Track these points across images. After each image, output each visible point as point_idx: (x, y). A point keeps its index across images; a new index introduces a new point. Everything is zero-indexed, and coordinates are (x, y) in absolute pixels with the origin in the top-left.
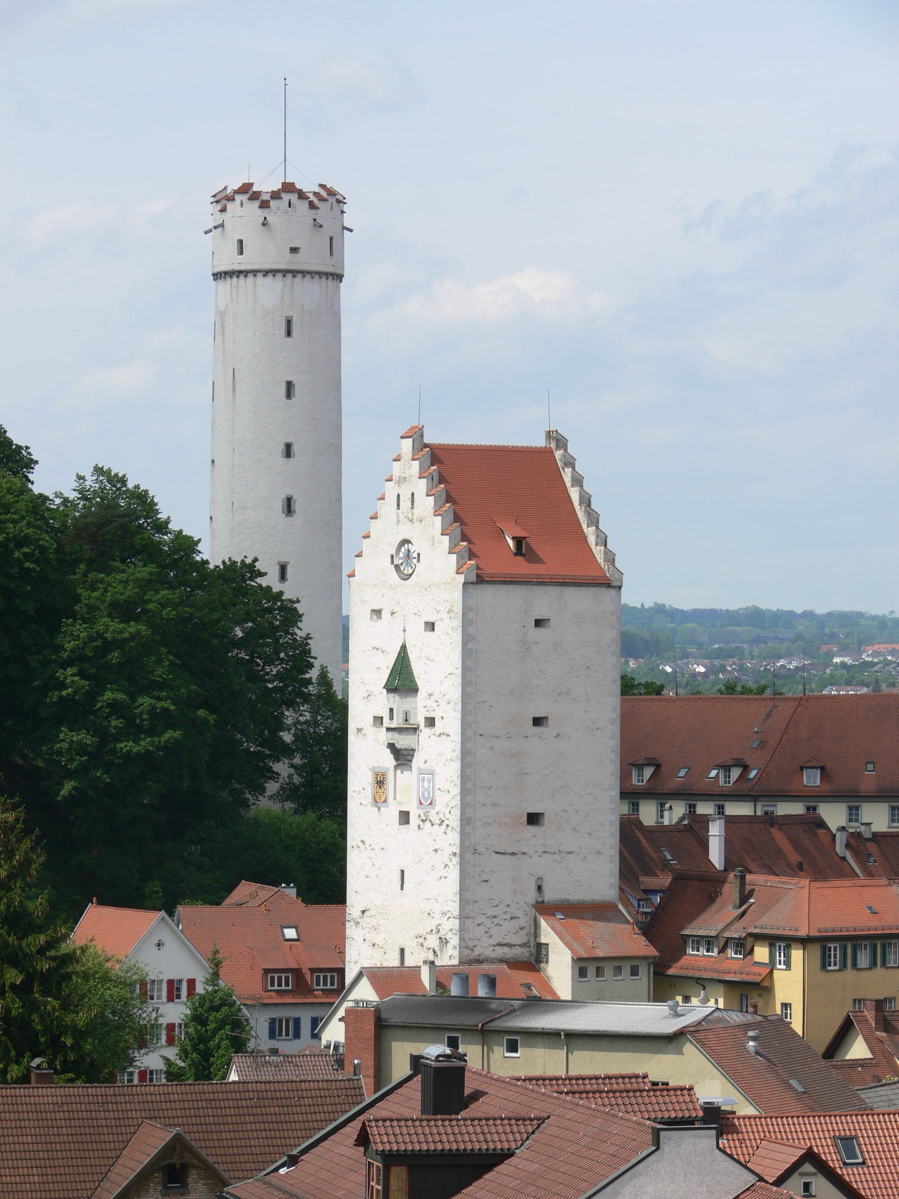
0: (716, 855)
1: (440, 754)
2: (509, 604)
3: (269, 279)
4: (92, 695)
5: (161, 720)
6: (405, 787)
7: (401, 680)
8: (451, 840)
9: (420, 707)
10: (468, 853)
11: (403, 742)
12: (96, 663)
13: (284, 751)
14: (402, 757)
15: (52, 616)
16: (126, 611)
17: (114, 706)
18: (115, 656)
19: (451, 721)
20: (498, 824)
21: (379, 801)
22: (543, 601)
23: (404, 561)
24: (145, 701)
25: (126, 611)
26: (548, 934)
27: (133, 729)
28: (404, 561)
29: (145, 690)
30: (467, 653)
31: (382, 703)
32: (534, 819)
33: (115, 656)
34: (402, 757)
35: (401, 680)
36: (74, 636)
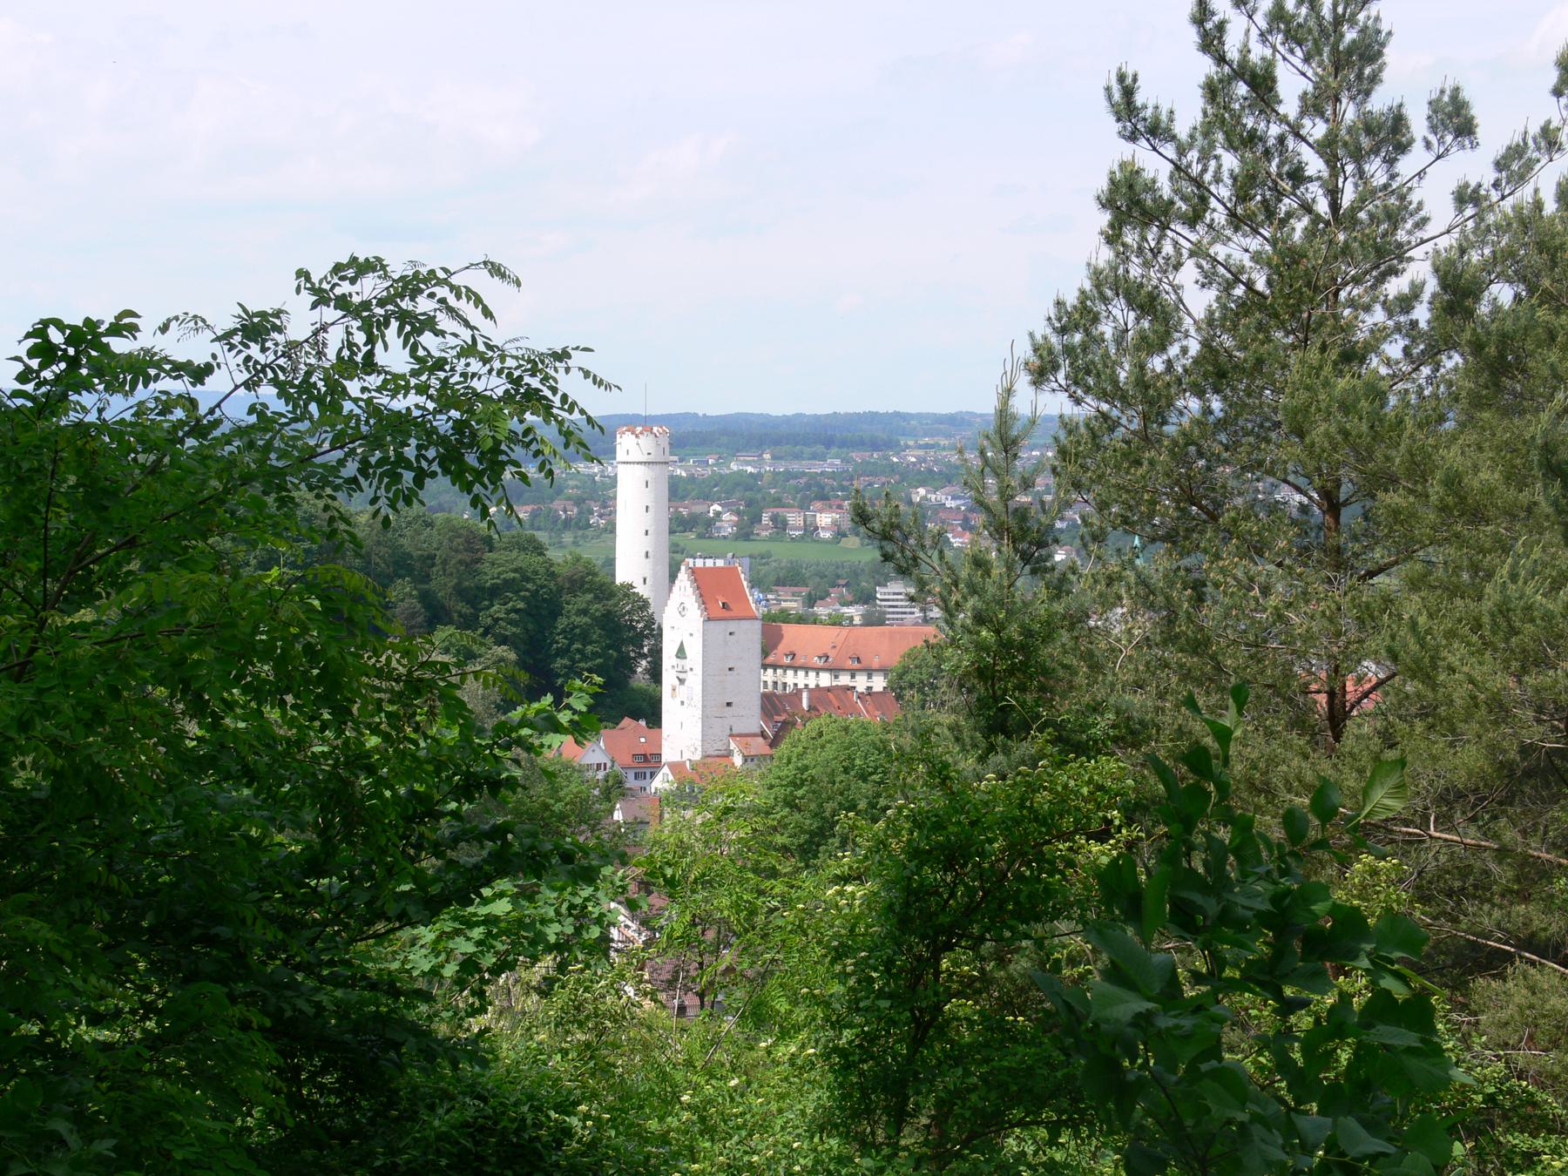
0: (805, 705)
1: (695, 681)
2: (720, 628)
3: (642, 467)
4: (570, 645)
5: (595, 655)
6: (681, 689)
7: (681, 653)
8: (699, 713)
9: (687, 664)
10: (705, 718)
11: (682, 676)
12: (570, 633)
13: (644, 656)
14: (682, 681)
15: (556, 612)
16: (584, 612)
17: (578, 650)
18: (577, 631)
19: (698, 670)
20: (717, 706)
21: (673, 696)
22: (732, 626)
23: (682, 609)
24: (589, 648)
25: (584, 612)
26: (733, 746)
27: (585, 658)
28: (682, 609)
29: (590, 643)
30: (704, 646)
31: (675, 661)
32: (729, 704)
33: (577, 631)
34: (682, 681)
35: (681, 653)
36: (562, 623)
